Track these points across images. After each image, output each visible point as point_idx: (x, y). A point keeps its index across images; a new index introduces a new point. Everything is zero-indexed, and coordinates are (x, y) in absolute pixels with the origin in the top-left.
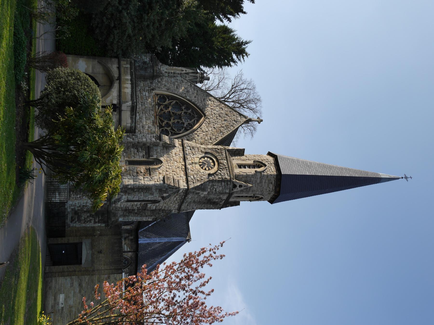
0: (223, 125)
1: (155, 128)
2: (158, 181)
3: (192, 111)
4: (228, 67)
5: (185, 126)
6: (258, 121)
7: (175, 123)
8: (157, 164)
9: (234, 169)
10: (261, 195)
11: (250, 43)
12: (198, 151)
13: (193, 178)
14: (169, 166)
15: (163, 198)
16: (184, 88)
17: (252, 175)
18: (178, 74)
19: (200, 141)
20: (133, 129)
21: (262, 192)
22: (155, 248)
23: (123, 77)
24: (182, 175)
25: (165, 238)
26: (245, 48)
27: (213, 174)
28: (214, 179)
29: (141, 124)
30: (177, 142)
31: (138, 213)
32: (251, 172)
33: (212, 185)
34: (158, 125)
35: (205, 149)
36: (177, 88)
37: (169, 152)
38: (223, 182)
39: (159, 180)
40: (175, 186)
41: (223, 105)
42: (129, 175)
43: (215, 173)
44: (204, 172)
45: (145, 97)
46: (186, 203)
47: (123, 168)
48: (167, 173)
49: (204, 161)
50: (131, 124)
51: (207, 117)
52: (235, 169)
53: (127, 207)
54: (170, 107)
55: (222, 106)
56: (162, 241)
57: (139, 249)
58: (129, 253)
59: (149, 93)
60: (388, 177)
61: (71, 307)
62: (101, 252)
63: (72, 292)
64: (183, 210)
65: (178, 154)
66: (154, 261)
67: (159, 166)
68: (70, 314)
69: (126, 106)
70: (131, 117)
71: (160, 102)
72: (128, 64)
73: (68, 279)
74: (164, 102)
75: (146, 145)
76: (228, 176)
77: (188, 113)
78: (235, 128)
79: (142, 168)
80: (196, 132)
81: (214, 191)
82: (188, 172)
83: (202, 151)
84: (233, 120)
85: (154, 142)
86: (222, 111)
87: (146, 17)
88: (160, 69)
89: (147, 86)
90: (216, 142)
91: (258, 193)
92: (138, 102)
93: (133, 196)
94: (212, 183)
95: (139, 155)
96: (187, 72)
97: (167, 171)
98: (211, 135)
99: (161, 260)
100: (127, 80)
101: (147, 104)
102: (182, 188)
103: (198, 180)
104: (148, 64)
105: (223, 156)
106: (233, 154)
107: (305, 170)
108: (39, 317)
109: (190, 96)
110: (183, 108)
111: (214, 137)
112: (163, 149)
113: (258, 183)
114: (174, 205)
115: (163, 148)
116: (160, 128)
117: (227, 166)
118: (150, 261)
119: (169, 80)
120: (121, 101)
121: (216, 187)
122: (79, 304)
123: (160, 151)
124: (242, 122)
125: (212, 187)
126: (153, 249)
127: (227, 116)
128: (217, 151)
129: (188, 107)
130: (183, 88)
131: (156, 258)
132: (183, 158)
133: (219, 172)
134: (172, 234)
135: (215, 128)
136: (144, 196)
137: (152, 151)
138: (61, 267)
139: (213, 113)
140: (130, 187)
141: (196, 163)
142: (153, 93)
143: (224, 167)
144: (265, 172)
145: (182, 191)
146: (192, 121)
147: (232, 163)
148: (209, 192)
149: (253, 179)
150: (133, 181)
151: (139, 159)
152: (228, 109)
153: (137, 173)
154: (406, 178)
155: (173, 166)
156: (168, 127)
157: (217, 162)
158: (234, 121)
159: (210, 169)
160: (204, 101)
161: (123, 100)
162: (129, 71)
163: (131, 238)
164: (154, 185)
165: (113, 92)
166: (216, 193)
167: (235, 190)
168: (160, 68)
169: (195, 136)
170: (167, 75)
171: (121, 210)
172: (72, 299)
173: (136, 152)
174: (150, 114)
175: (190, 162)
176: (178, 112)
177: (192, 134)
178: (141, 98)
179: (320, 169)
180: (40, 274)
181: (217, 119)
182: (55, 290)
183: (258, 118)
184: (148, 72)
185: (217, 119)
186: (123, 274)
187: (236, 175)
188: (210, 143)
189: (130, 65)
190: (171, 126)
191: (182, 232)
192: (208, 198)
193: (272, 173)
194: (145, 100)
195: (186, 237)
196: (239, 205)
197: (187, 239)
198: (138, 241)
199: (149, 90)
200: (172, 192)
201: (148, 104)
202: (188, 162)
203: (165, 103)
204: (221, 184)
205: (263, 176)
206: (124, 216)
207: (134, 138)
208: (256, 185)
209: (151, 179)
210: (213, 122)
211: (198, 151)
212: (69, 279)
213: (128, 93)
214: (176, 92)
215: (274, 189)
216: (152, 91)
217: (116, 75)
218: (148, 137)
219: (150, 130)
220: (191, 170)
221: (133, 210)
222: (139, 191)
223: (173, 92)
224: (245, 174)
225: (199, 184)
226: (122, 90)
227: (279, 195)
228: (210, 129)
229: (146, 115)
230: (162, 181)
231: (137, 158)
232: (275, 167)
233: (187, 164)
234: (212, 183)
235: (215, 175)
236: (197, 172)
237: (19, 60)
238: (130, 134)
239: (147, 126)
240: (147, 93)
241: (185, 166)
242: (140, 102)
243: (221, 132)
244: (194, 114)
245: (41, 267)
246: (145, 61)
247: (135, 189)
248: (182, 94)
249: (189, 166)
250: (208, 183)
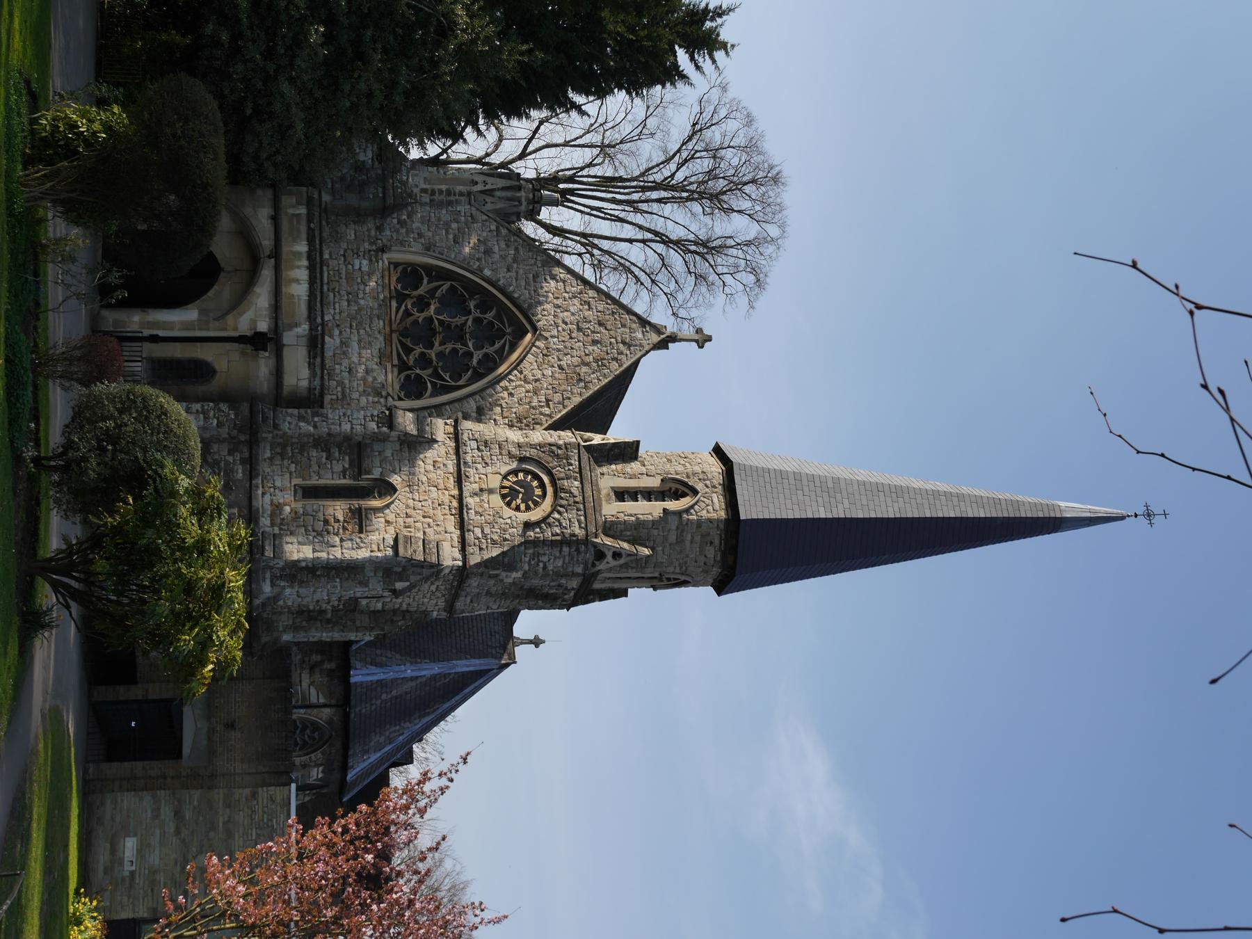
0: (588, 359)
1: (386, 372)
2: (379, 550)
3: (498, 317)
4: (664, 86)
5: (475, 361)
6: (697, 341)
7: (445, 355)
8: (381, 496)
9: (600, 506)
10: (682, 574)
12: (501, 454)
13: (480, 536)
14: (414, 500)
15: (396, 593)
16: (478, 240)
17: (654, 522)
18: (461, 194)
19: (514, 410)
20: (315, 395)
21: (684, 568)
22: (401, 695)
24: (451, 528)
25: (432, 665)
26: (716, 27)
27: (537, 524)
28: (538, 538)
29: (345, 363)
30: (441, 428)
31: (334, 620)
32: (651, 514)
33: (534, 554)
34: (396, 362)
35: (519, 446)
36: (455, 242)
37: (416, 459)
38: (564, 546)
39: (382, 547)
40: (429, 560)
41: (592, 293)
42: (303, 530)
43: (544, 520)
44: (514, 518)
46: (466, 596)
47: (287, 509)
48: (408, 520)
49: (514, 483)
50: (310, 382)
51: (540, 334)
52: (604, 503)
53: (303, 605)
54: (433, 302)
55: (590, 295)
56: (423, 673)
57: (352, 698)
58: (323, 710)
59: (370, 260)
60: (1088, 515)
61: (155, 872)
62: (233, 726)
63: (158, 832)
64: (463, 612)
65: (442, 465)
66: (399, 730)
67: (388, 500)
68: (152, 890)
69: (295, 337)
70: (309, 363)
71: (404, 288)
72: (301, 204)
73: (147, 798)
74: (416, 288)
75: (351, 439)
76: (580, 527)
77: (485, 322)
78: (625, 366)
79: (338, 509)
80: (504, 383)
81: (541, 570)
82: (466, 518)
83: (510, 455)
84: (619, 339)
85: (375, 433)
86: (587, 313)
87: (347, 88)
88: (405, 183)
89: (366, 239)
90: (564, 412)
91: (671, 569)
92: (338, 292)
93: (312, 590)
94: (535, 547)
95: (331, 468)
96: (488, 187)
97: (408, 516)
98: (548, 392)
99: (419, 726)
100: (298, 255)
101: (363, 298)
102: (447, 566)
103: (494, 542)
105: (571, 468)
106: (604, 457)
107: (814, 504)
108: (73, 903)
109: (494, 267)
110: (472, 304)
111: (558, 397)
112: (401, 450)
113: (670, 545)
114: (435, 601)
115: (401, 445)
117: (579, 499)
118: (385, 731)
119: (433, 215)
120: (280, 322)
121: (545, 559)
122: (176, 864)
123: (392, 455)
124: (647, 348)
125: (534, 559)
126: (396, 697)
128: (553, 452)
129: (487, 302)
130: (474, 240)
131: (405, 723)
132: (455, 475)
133: (556, 515)
134: (454, 651)
135: (563, 369)
136: (341, 587)
137: (368, 457)
138: (127, 765)
139: (560, 321)
140: (304, 564)
141: (491, 491)
142: (383, 261)
143: (571, 500)
144: (692, 511)
145: (450, 572)
146: (497, 346)
147: (597, 485)
148: (525, 572)
149: (655, 532)
150: (311, 551)
151: (333, 482)
152: (607, 304)
153: (326, 522)
154: (1149, 515)
155: (426, 500)
156: (425, 369)
157: (553, 486)
158: (624, 343)
159: (532, 506)
160: (535, 281)
161: (285, 319)
163: (327, 666)
164: (371, 561)
165: (259, 295)
167: (601, 566)
168: (405, 178)
169: (502, 394)
170: (426, 198)
171: (288, 612)
172: (157, 852)
173: (324, 460)
174: (371, 329)
175: (476, 487)
176: (457, 319)
177: (494, 390)
178: (346, 278)
179: (864, 498)
180: (74, 791)
181: (571, 338)
182: (112, 826)
183: (697, 332)
184: (369, 198)
185: (571, 338)
186: (293, 786)
187: (605, 522)
188: (545, 415)
189: (309, 209)
190: (435, 363)
191: (489, 643)
192: (527, 585)
193: (714, 515)
194: (358, 284)
195: (501, 658)
196: (626, 596)
197: (503, 662)
198: (350, 676)
199: (372, 253)
200: (418, 577)
201: (368, 298)
202: (468, 487)
203: (421, 291)
204: (560, 552)
205: (687, 524)
206: (295, 628)
207: (318, 424)
208: (667, 550)
209: (362, 545)
210: (559, 350)
211: (501, 454)
212: (149, 798)
213: (298, 296)
214: (453, 256)
215: (719, 558)
216: (380, 253)
217: (267, 243)
218: (358, 419)
219: (370, 379)
220: (476, 513)
221: (322, 612)
222: (328, 575)
223: (444, 257)
224: (633, 519)
225: (495, 552)
226: (284, 289)
228: (548, 372)
229: (362, 332)
230: (392, 547)
231: (327, 480)
232: (725, 497)
233: (466, 494)
234: (535, 547)
235: (543, 525)
236: (492, 518)
237: (18, 409)
238: (306, 412)
239: (363, 367)
240: (365, 262)
241: (460, 499)
242: (343, 293)
243: (580, 380)
244: (503, 324)
245: (74, 783)
246: (361, 159)
247: (317, 570)
248: (469, 263)
249: (470, 501)
250: (523, 548)
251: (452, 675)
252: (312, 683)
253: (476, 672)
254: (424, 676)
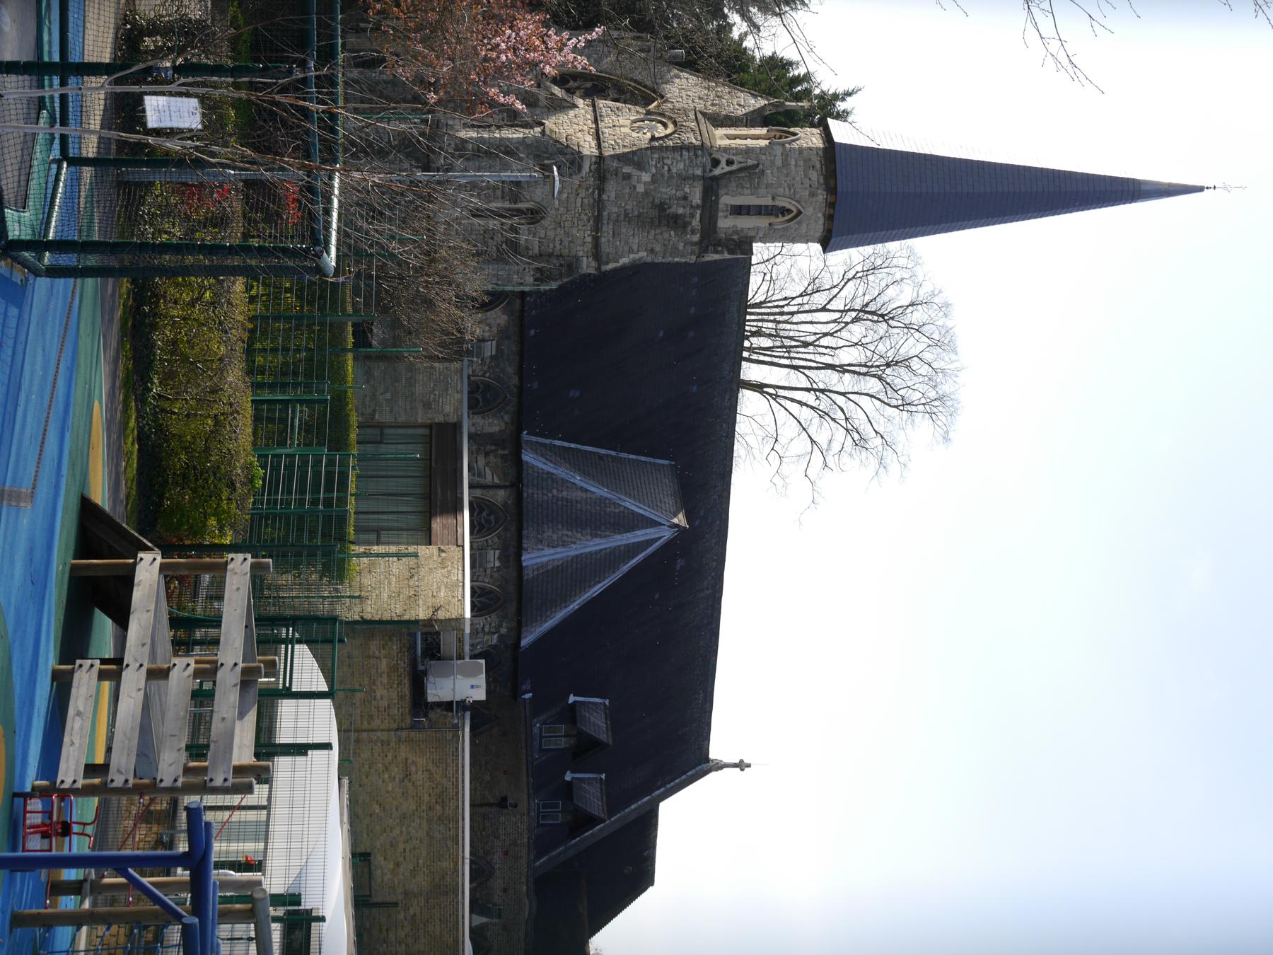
11: (859, 92)
113: (778, 168)
121: (668, 162)
149: (764, 157)
163: (501, 452)
166: (671, 177)
215: (822, 181)
251: (622, 509)
252: (487, 464)
253: (647, 541)
254: (594, 493)
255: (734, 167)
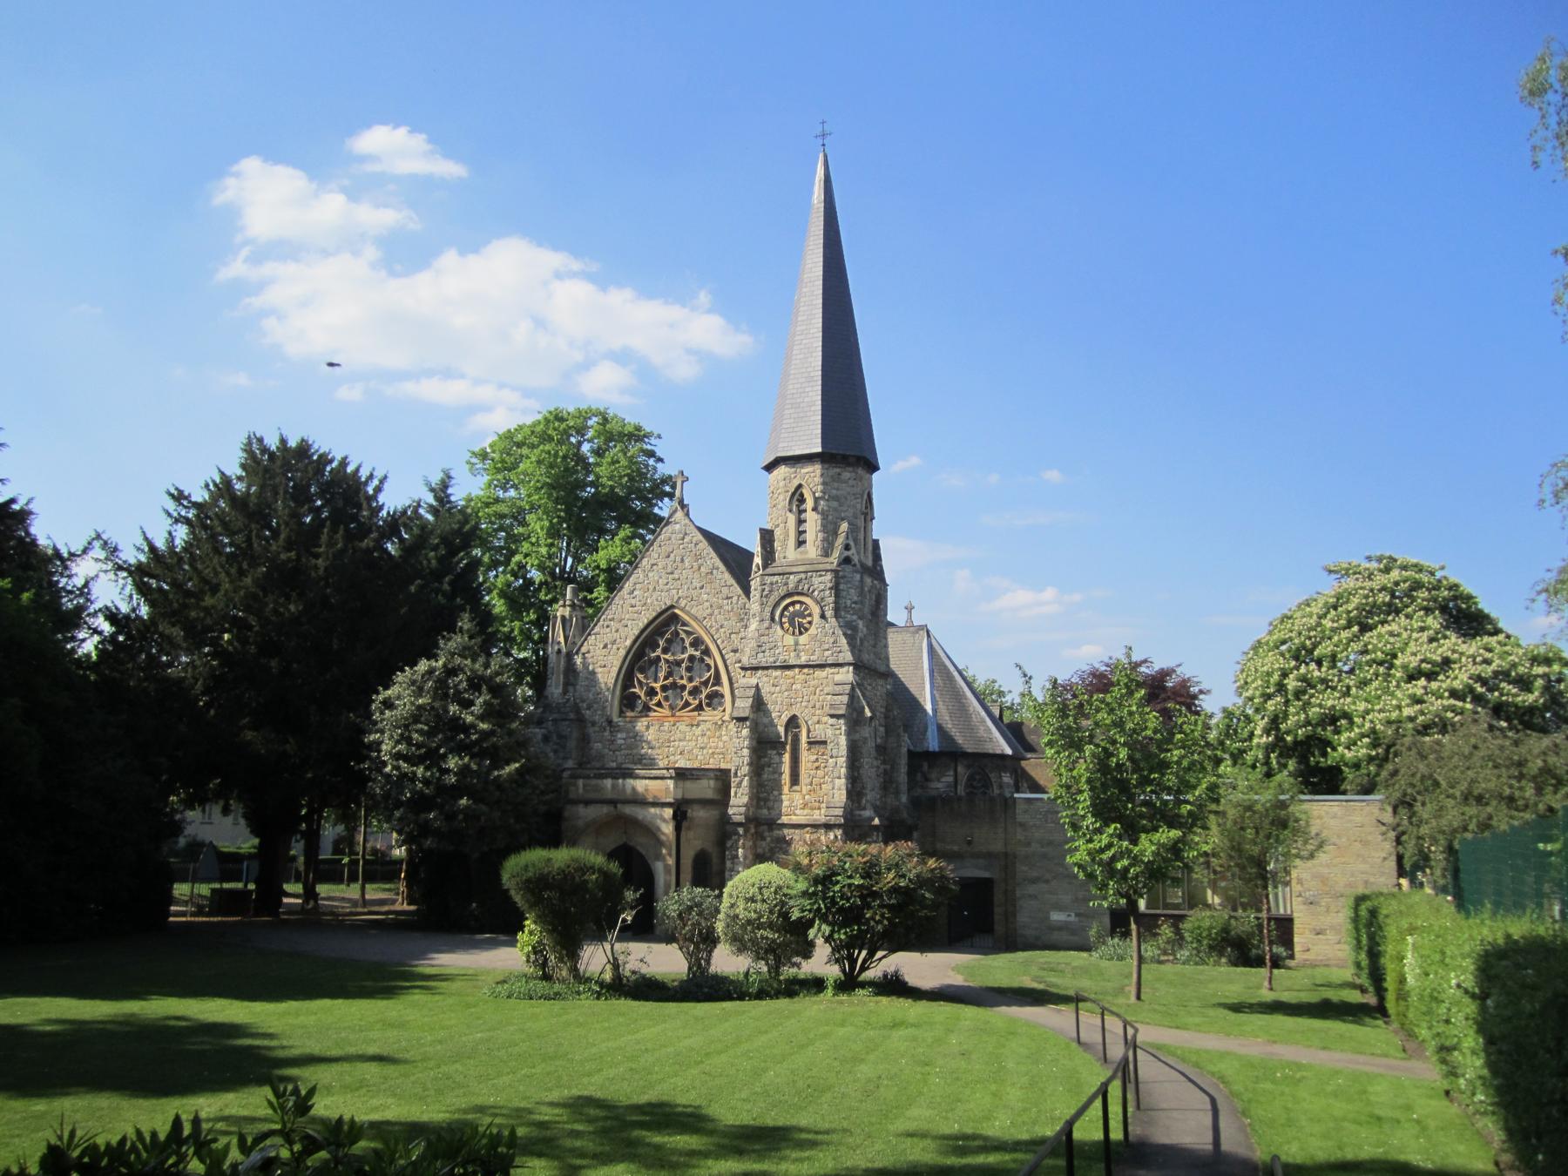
0: (696, 567)
9: (808, 560)
17: (823, 519)
23: (609, 795)
34: (696, 713)
45: (629, 741)
52: (807, 556)
59: (618, 731)
86: (660, 567)
97: (814, 707)
100: (614, 786)
104: (549, 732)
116: (703, 710)
121: (849, 602)
127: (672, 555)
133: (816, 593)
141: (797, 644)
149: (830, 517)
162: (594, 782)
164: (849, 734)
167: (855, 559)
186: (1016, 795)
189: (580, 777)
193: (818, 472)
206: (897, 793)
215: (851, 469)
225: (844, 641)
227: (864, 458)
240: (619, 736)
241: (802, 667)
243: (712, 573)
252: (939, 781)
255: (852, 544)
